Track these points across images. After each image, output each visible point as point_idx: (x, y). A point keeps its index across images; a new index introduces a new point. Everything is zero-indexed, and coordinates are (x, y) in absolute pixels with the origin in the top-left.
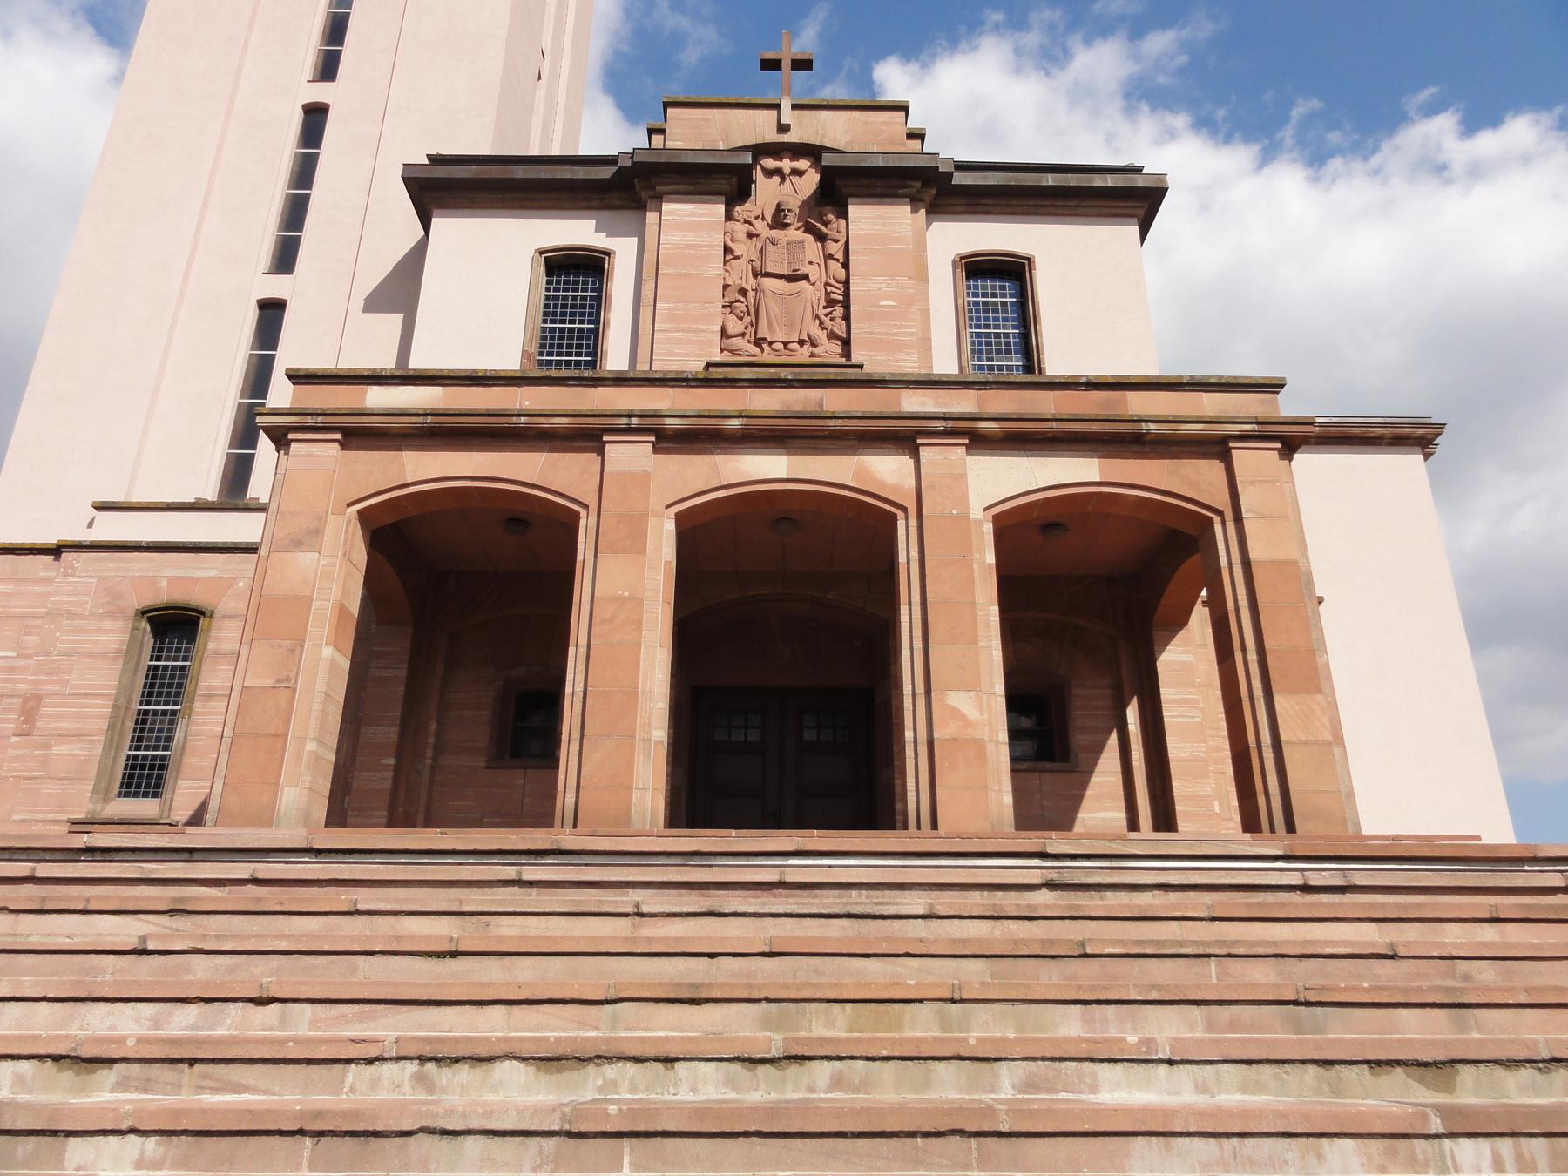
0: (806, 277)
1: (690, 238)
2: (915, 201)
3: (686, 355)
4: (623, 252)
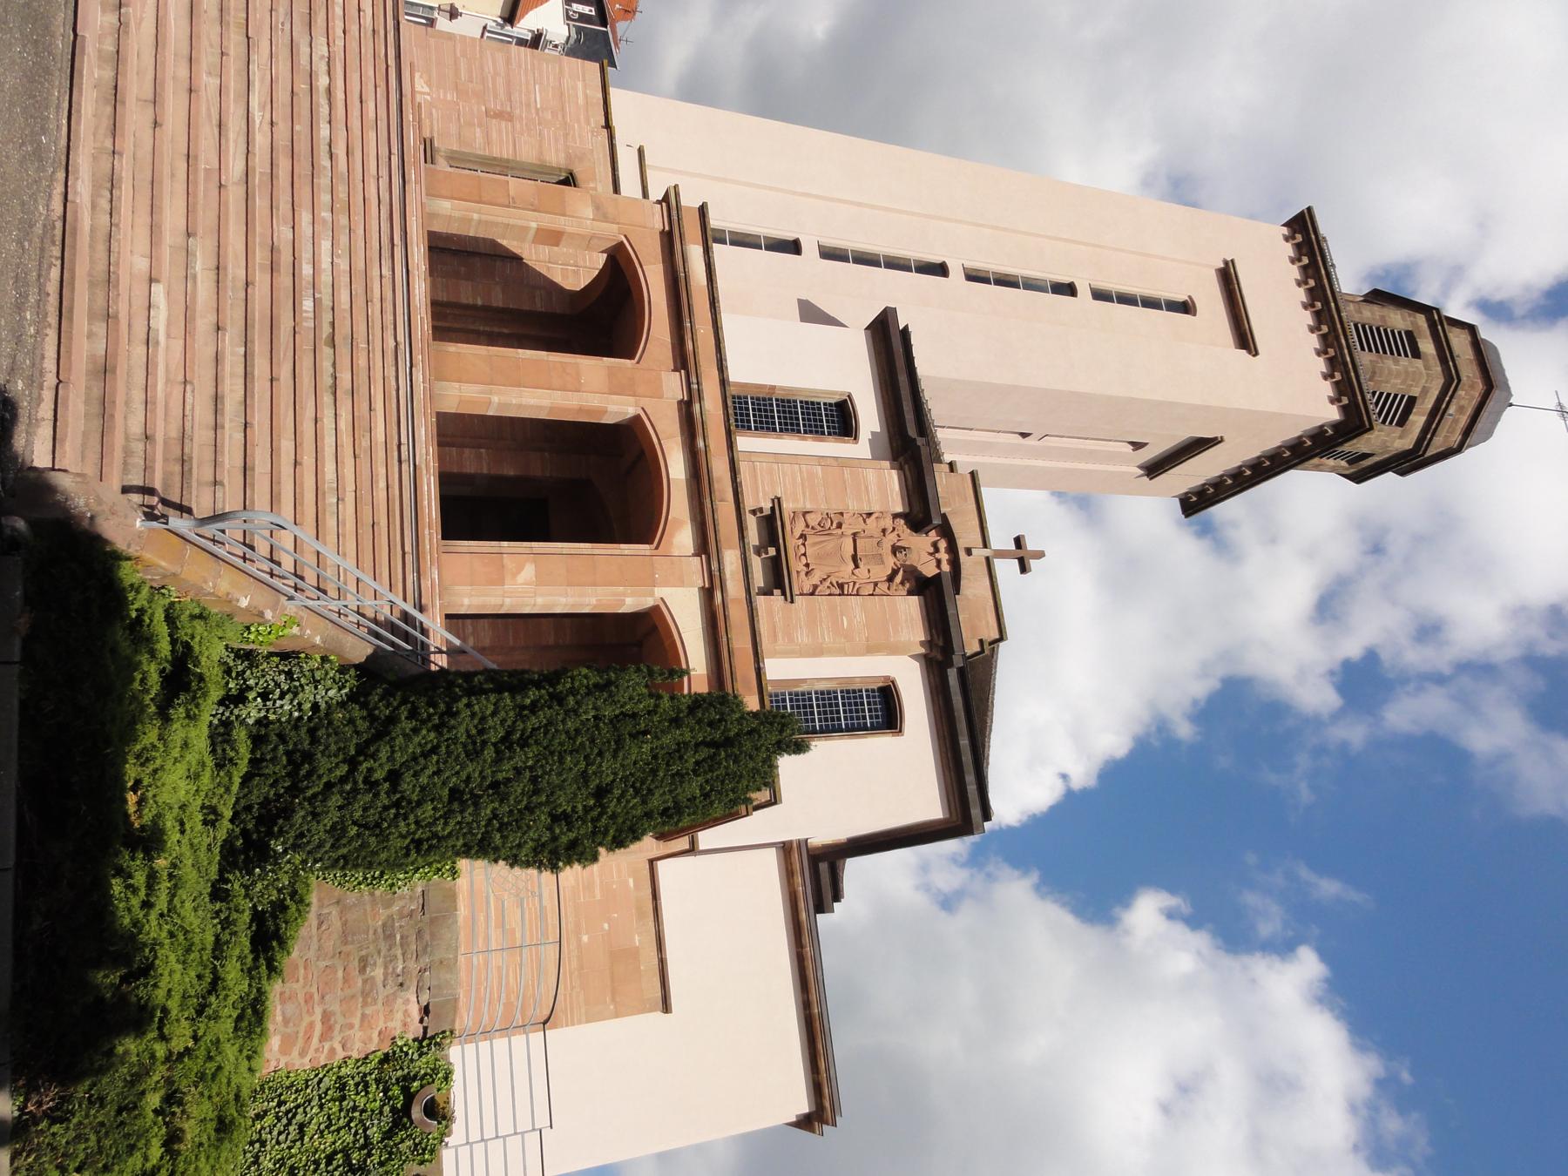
0: (857, 566)
1: (873, 488)
2: (929, 644)
4: (860, 449)
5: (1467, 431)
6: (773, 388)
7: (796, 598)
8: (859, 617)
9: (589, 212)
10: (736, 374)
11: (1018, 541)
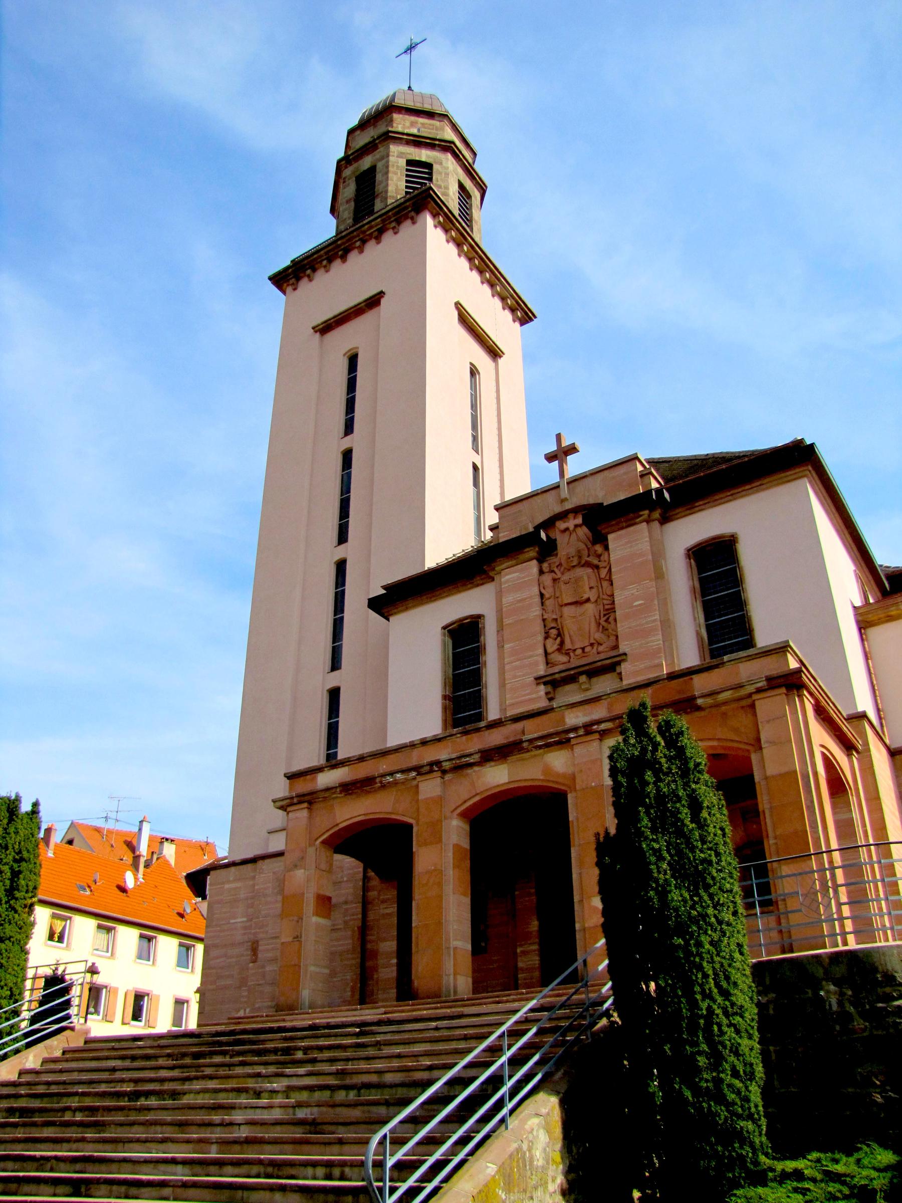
1: (519, 596)
3: (524, 675)
5: (430, 115)
6: (445, 697)
7: (621, 651)
8: (633, 590)
9: (300, 873)
10: (845, 715)
11: (550, 458)
